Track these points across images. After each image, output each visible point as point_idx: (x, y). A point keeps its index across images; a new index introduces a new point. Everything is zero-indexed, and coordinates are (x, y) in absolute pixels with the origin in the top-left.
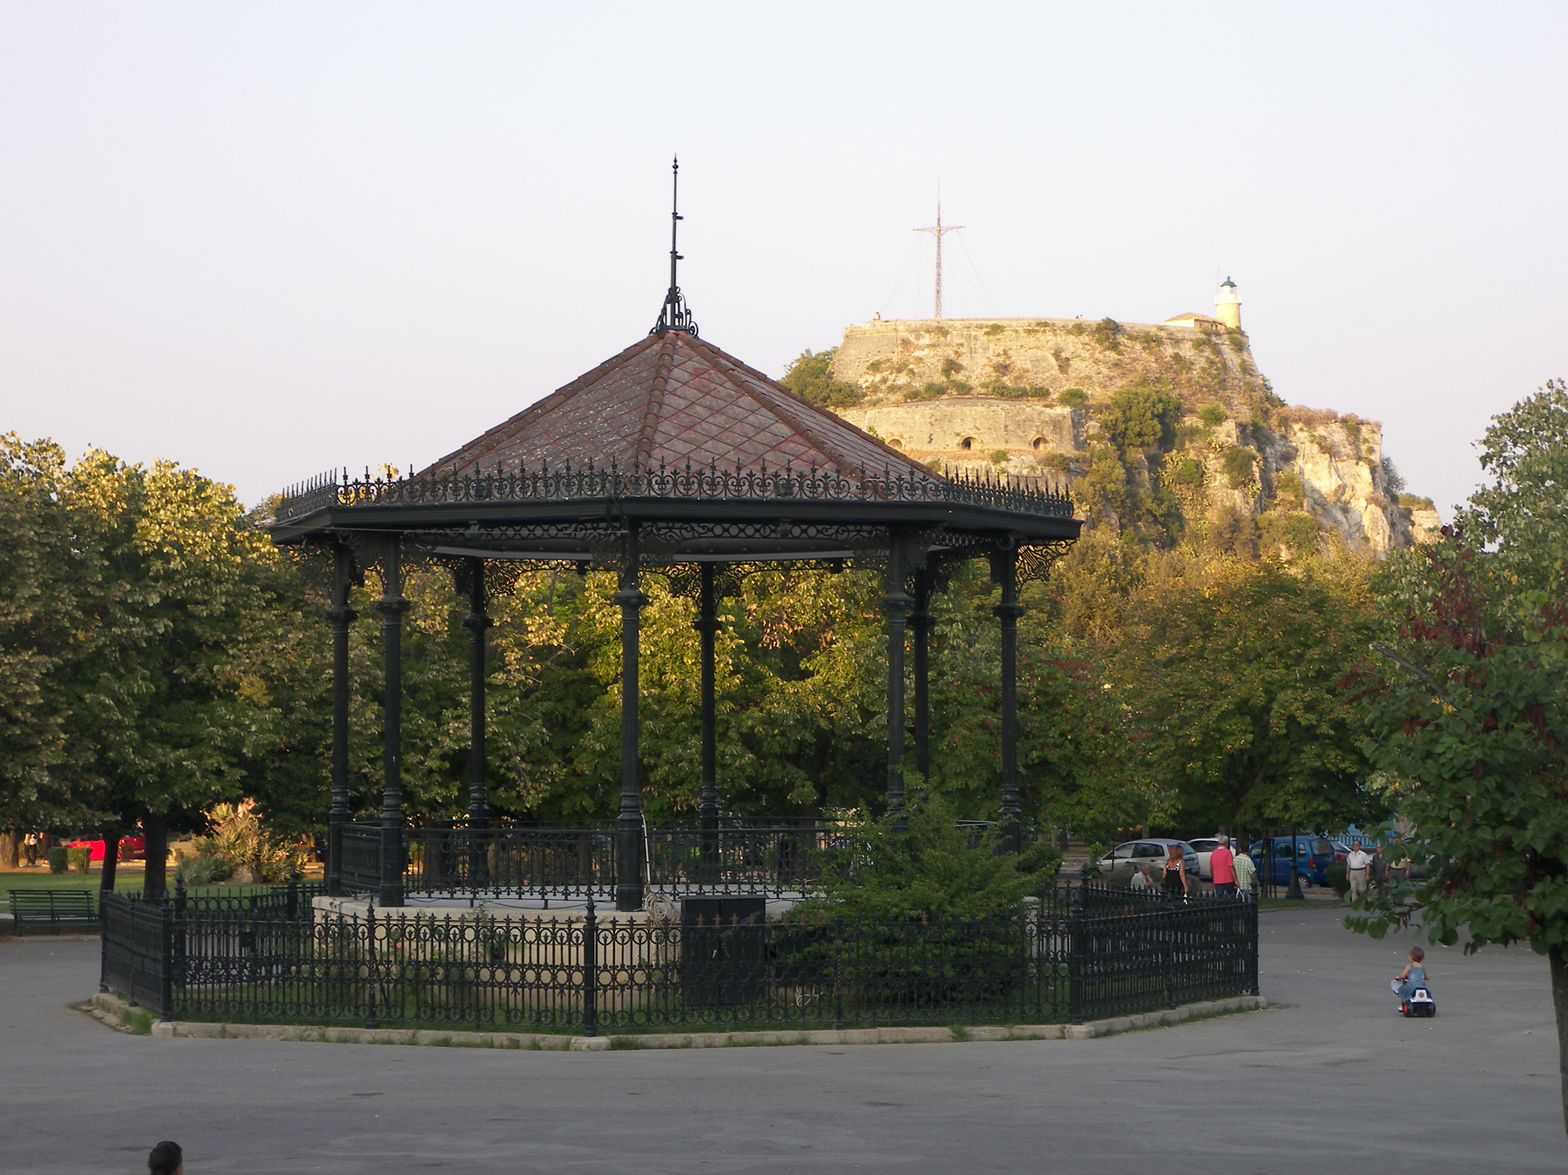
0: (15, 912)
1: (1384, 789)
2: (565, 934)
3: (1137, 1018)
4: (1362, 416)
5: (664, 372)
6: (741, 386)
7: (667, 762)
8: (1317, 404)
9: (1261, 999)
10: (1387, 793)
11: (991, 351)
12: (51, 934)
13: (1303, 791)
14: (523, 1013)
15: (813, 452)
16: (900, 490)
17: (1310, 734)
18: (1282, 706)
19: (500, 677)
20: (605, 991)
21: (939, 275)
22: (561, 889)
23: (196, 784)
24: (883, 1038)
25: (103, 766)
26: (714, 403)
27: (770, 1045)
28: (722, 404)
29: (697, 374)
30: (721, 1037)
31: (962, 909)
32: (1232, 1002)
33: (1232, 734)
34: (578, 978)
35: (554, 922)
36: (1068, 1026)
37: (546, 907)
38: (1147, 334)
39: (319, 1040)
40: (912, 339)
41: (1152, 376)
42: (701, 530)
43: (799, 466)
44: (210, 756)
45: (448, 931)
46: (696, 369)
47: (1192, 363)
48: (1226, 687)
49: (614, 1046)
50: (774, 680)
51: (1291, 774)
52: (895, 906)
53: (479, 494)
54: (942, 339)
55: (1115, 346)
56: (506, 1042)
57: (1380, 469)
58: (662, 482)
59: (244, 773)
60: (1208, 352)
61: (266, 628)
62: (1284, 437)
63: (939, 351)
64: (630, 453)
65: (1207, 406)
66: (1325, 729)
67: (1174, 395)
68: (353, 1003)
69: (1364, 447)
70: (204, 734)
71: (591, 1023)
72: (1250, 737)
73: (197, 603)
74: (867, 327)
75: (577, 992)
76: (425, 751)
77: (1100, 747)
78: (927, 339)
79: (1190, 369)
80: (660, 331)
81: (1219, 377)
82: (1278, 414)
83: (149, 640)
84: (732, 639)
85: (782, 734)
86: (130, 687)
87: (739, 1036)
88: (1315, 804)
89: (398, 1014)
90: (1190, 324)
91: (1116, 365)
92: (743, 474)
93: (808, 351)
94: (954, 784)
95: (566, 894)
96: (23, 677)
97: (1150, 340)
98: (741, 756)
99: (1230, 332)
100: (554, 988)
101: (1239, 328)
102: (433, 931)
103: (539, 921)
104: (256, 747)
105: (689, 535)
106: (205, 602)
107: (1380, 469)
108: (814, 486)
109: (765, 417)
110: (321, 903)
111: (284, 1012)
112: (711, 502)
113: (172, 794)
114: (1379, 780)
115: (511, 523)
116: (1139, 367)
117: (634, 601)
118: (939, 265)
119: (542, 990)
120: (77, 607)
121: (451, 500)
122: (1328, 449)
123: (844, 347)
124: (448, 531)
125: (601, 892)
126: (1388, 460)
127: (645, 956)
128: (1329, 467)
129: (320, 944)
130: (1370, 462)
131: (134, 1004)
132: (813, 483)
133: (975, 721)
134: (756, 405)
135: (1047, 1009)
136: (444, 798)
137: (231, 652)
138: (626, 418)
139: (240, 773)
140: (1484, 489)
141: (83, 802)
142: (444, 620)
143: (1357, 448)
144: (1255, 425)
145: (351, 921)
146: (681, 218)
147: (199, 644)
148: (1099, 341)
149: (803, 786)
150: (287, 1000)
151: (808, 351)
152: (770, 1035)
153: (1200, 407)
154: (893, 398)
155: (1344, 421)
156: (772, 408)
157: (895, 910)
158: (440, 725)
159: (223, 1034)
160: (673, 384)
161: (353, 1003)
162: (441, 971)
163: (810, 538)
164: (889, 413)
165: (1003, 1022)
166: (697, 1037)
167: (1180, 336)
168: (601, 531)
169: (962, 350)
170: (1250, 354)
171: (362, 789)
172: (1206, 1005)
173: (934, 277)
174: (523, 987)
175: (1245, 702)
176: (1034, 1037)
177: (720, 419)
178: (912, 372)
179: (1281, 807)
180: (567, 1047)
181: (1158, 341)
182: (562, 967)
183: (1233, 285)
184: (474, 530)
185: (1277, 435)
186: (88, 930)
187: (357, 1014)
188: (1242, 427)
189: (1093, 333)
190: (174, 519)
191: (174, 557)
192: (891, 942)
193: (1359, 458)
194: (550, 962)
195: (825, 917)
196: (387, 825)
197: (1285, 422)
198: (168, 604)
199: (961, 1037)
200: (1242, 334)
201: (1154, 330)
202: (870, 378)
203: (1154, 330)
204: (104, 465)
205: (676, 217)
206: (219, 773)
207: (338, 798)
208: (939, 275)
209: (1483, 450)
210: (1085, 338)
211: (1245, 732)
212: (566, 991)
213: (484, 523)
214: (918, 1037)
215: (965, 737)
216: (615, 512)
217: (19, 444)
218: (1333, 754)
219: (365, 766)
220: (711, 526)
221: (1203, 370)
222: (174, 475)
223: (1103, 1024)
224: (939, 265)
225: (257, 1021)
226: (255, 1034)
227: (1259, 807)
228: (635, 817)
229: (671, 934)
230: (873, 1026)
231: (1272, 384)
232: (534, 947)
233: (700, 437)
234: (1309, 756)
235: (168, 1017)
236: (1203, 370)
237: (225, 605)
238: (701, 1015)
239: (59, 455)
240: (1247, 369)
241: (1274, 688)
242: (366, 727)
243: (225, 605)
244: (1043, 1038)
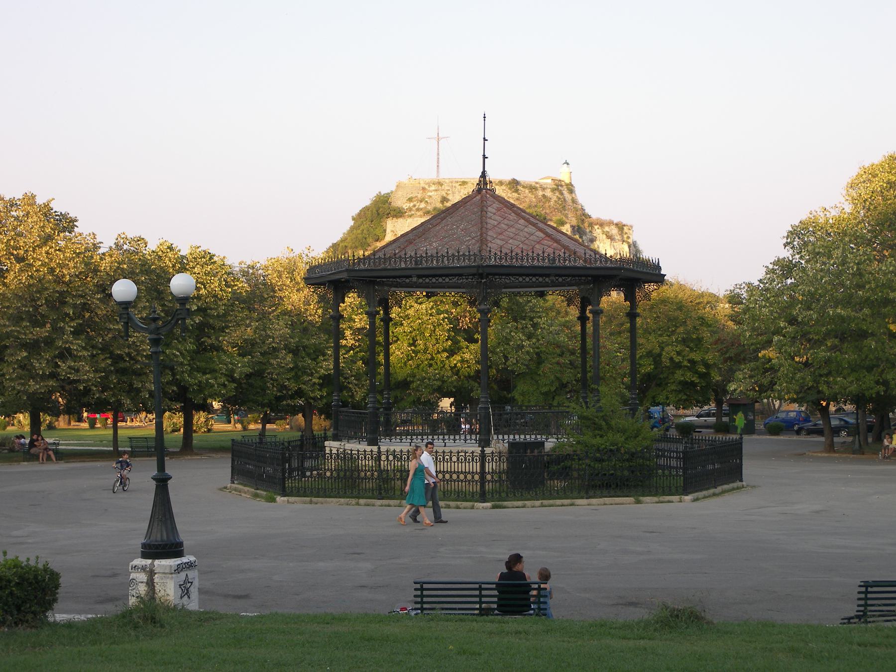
0: (131, 447)
1: (735, 390)
2: (441, 458)
3: (705, 493)
4: (624, 223)
5: (485, 209)
6: (518, 215)
7: (418, 380)
8: (605, 216)
9: (744, 483)
10: (737, 392)
11: (462, 193)
12: (145, 457)
13: (676, 390)
14: (451, 493)
15: (555, 244)
16: (601, 262)
17: (678, 366)
18: (667, 353)
19: (344, 342)
20: (489, 483)
21: (438, 158)
22: (452, 437)
23: (215, 390)
24: (606, 503)
25: (175, 382)
26: (508, 222)
27: (559, 506)
28: (512, 223)
29: (498, 210)
30: (538, 503)
31: (631, 446)
32: (731, 485)
33: (644, 365)
34: (477, 477)
35: (451, 452)
36: (683, 497)
37: (445, 446)
38: (531, 185)
39: (356, 505)
40: (427, 187)
41: (533, 204)
42: (513, 279)
43: (550, 250)
44: (221, 378)
45: (401, 457)
46: (498, 208)
47: (551, 199)
48: (642, 345)
49: (494, 507)
50: (464, 344)
51: (669, 383)
52: (602, 445)
53: (416, 263)
54: (440, 187)
55: (517, 191)
56: (444, 506)
57: (632, 246)
58: (512, 258)
59: (236, 385)
60: (557, 194)
61: (241, 320)
62: (591, 232)
63: (439, 193)
64: (478, 245)
65: (558, 218)
66: (686, 363)
67: (543, 212)
68: (357, 488)
69: (625, 236)
70: (217, 368)
71: (483, 497)
72: (652, 367)
73: (211, 309)
74: (406, 182)
75: (476, 483)
76: (312, 375)
77: (606, 372)
78: (433, 188)
79: (550, 201)
80: (479, 191)
81: (562, 205)
82: (588, 221)
83: (192, 325)
84: (447, 325)
85: (468, 367)
86: (185, 347)
87: (546, 502)
88: (680, 396)
89: (392, 493)
90: (549, 181)
91: (517, 199)
92: (546, 255)
93: (380, 193)
94: (545, 389)
95: (455, 440)
96: (142, 342)
97: (532, 188)
98: (452, 377)
99: (567, 185)
100: (465, 482)
101: (571, 183)
102: (394, 457)
103: (444, 452)
104: (241, 373)
105: (508, 281)
106: (214, 309)
107: (632, 246)
108: (543, 260)
109: (531, 229)
110: (332, 446)
111: (339, 493)
112: (522, 267)
113: (204, 394)
114: (733, 386)
115: (427, 276)
116: (527, 200)
117: (486, 311)
118: (438, 154)
119: (460, 483)
120: (162, 311)
121: (403, 266)
122: (610, 237)
123: (396, 191)
124: (398, 280)
125: (471, 439)
126: (635, 242)
127: (494, 468)
128: (611, 245)
129: (335, 462)
130: (628, 243)
131: (257, 489)
132: (543, 257)
133: (554, 361)
134: (527, 224)
135: (673, 490)
136: (321, 396)
137: (227, 331)
138: (472, 229)
139: (234, 385)
140: (778, 259)
141: (166, 398)
142: (319, 317)
143: (623, 236)
144: (578, 226)
145: (349, 452)
146: (487, 140)
147: (212, 327)
148: (510, 189)
149: (477, 390)
150: (320, 487)
151: (380, 193)
152: (558, 502)
153: (554, 218)
154: (419, 213)
155: (617, 224)
156: (534, 225)
157: (603, 446)
158: (317, 364)
159: (311, 502)
160: (489, 214)
161: (357, 488)
162: (399, 474)
163: (533, 282)
164: (417, 220)
165: (655, 495)
166: (528, 503)
167: (545, 186)
168: (470, 280)
169: (449, 192)
170: (575, 194)
171: (284, 392)
172: (726, 487)
173: (436, 158)
174: (451, 481)
175: (650, 352)
176: (669, 502)
177: (513, 230)
178: (427, 201)
179: (665, 397)
180: (472, 508)
181: (536, 189)
182: (454, 472)
183: (568, 164)
184: (415, 279)
185: (588, 230)
186: (149, 455)
187: (373, 493)
188: (573, 227)
189: (507, 185)
190: (202, 272)
191: (202, 289)
192: (600, 460)
193: (624, 241)
194: (456, 470)
195: (569, 450)
196: (371, 410)
197: (591, 225)
198: (200, 310)
199: (638, 502)
200: (572, 185)
201: (534, 184)
202: (408, 205)
203: (534, 184)
204: (169, 248)
205: (485, 140)
206: (224, 385)
207: (336, 398)
208: (438, 158)
209: (785, 241)
210: (504, 187)
211: (650, 365)
212: (471, 483)
213: (419, 277)
214: (620, 502)
215: (550, 368)
216: (481, 271)
217: (126, 238)
218: (689, 374)
219: (286, 382)
220: (517, 277)
221: (555, 201)
222: (200, 252)
223: (696, 495)
224: (438, 154)
225: (326, 497)
226: (326, 502)
227: (654, 397)
228: (487, 406)
229: (502, 458)
230: (601, 498)
231: (585, 208)
232: (456, 464)
233: (506, 238)
234: (679, 375)
235: (284, 494)
236: (555, 201)
237: (224, 310)
238: (529, 493)
239: (146, 244)
240: (574, 201)
241: (663, 345)
242: (287, 365)
243: (224, 310)
244: (672, 502)
